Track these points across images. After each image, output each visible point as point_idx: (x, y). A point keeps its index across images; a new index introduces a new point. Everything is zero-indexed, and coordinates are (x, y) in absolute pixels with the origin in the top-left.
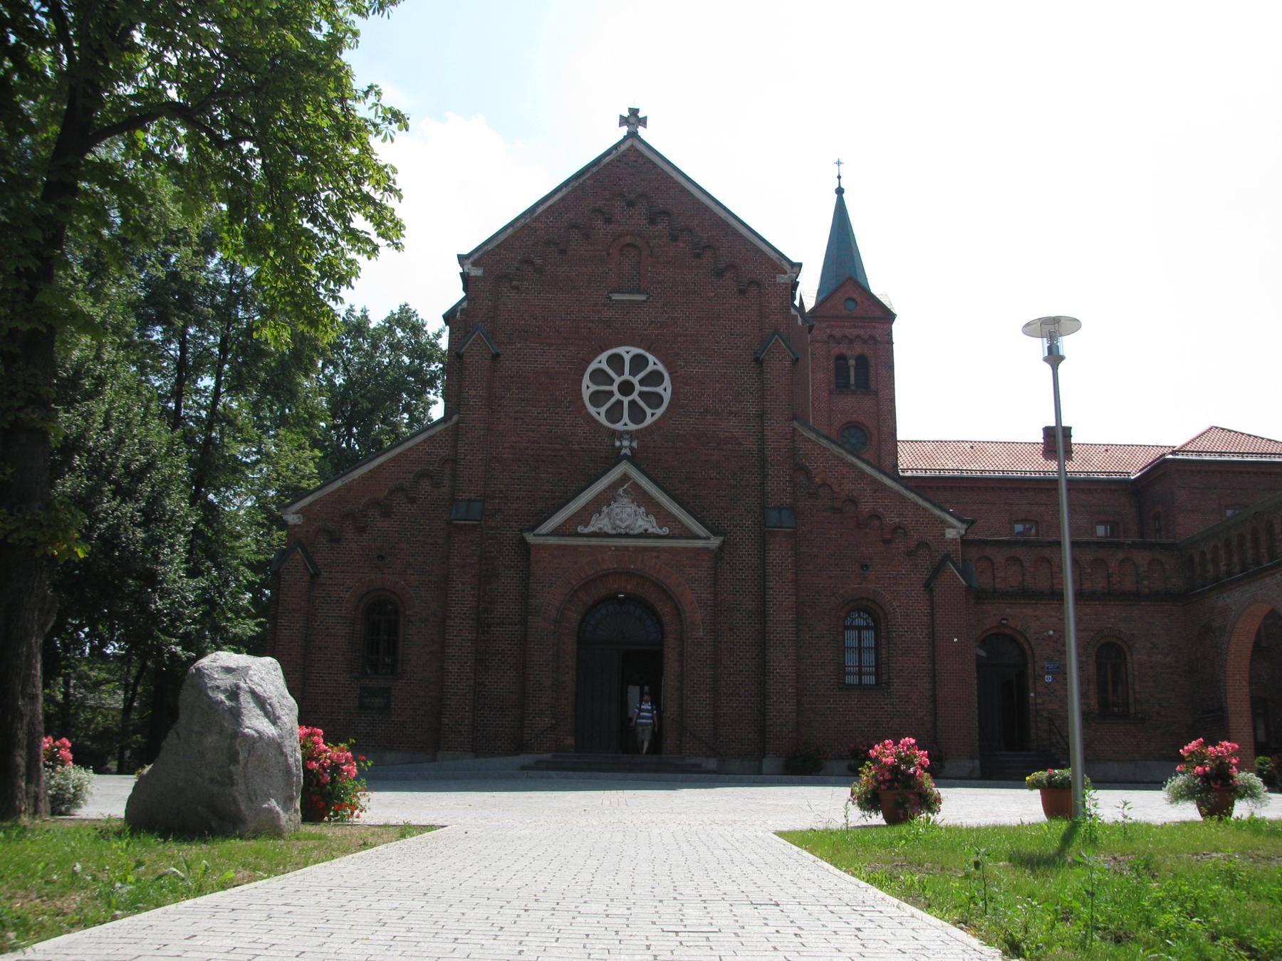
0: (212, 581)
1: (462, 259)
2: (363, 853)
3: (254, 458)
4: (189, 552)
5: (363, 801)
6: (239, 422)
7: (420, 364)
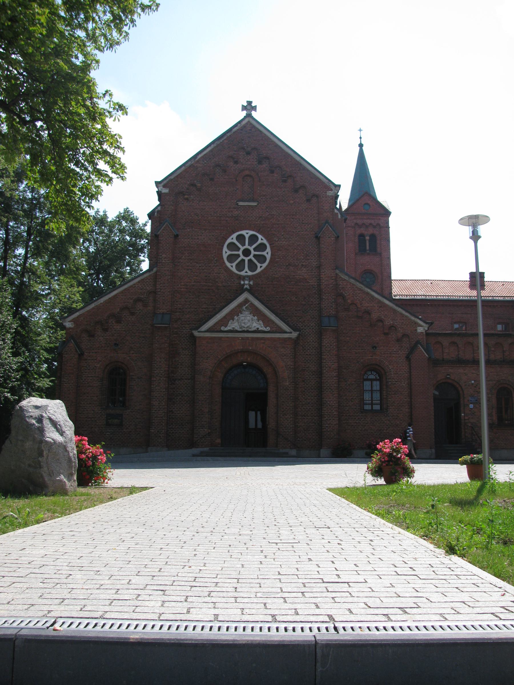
0: (26, 359)
1: (157, 183)
2: (110, 503)
3: (47, 292)
4: (13, 343)
5: (110, 475)
6: (38, 273)
7: (136, 240)
